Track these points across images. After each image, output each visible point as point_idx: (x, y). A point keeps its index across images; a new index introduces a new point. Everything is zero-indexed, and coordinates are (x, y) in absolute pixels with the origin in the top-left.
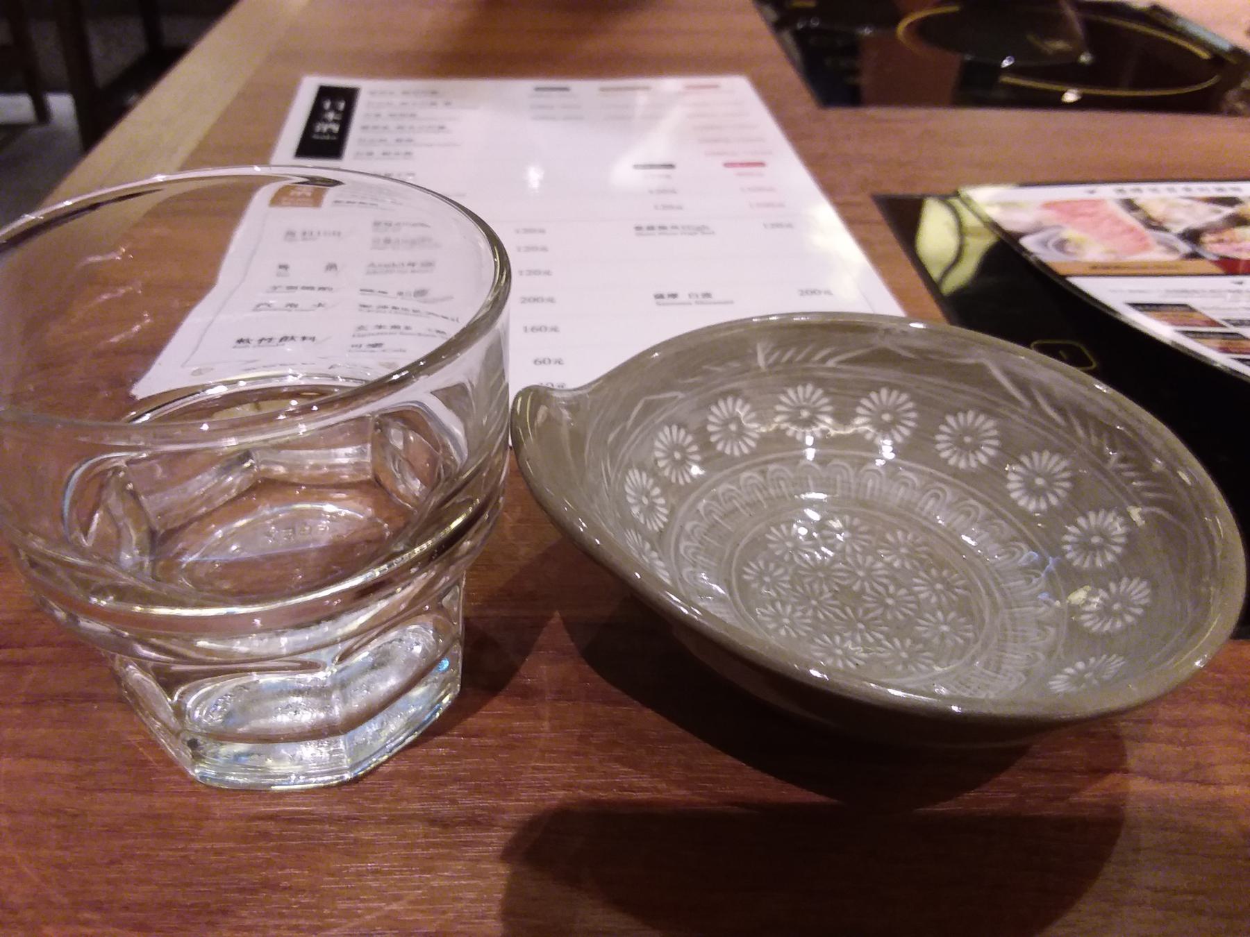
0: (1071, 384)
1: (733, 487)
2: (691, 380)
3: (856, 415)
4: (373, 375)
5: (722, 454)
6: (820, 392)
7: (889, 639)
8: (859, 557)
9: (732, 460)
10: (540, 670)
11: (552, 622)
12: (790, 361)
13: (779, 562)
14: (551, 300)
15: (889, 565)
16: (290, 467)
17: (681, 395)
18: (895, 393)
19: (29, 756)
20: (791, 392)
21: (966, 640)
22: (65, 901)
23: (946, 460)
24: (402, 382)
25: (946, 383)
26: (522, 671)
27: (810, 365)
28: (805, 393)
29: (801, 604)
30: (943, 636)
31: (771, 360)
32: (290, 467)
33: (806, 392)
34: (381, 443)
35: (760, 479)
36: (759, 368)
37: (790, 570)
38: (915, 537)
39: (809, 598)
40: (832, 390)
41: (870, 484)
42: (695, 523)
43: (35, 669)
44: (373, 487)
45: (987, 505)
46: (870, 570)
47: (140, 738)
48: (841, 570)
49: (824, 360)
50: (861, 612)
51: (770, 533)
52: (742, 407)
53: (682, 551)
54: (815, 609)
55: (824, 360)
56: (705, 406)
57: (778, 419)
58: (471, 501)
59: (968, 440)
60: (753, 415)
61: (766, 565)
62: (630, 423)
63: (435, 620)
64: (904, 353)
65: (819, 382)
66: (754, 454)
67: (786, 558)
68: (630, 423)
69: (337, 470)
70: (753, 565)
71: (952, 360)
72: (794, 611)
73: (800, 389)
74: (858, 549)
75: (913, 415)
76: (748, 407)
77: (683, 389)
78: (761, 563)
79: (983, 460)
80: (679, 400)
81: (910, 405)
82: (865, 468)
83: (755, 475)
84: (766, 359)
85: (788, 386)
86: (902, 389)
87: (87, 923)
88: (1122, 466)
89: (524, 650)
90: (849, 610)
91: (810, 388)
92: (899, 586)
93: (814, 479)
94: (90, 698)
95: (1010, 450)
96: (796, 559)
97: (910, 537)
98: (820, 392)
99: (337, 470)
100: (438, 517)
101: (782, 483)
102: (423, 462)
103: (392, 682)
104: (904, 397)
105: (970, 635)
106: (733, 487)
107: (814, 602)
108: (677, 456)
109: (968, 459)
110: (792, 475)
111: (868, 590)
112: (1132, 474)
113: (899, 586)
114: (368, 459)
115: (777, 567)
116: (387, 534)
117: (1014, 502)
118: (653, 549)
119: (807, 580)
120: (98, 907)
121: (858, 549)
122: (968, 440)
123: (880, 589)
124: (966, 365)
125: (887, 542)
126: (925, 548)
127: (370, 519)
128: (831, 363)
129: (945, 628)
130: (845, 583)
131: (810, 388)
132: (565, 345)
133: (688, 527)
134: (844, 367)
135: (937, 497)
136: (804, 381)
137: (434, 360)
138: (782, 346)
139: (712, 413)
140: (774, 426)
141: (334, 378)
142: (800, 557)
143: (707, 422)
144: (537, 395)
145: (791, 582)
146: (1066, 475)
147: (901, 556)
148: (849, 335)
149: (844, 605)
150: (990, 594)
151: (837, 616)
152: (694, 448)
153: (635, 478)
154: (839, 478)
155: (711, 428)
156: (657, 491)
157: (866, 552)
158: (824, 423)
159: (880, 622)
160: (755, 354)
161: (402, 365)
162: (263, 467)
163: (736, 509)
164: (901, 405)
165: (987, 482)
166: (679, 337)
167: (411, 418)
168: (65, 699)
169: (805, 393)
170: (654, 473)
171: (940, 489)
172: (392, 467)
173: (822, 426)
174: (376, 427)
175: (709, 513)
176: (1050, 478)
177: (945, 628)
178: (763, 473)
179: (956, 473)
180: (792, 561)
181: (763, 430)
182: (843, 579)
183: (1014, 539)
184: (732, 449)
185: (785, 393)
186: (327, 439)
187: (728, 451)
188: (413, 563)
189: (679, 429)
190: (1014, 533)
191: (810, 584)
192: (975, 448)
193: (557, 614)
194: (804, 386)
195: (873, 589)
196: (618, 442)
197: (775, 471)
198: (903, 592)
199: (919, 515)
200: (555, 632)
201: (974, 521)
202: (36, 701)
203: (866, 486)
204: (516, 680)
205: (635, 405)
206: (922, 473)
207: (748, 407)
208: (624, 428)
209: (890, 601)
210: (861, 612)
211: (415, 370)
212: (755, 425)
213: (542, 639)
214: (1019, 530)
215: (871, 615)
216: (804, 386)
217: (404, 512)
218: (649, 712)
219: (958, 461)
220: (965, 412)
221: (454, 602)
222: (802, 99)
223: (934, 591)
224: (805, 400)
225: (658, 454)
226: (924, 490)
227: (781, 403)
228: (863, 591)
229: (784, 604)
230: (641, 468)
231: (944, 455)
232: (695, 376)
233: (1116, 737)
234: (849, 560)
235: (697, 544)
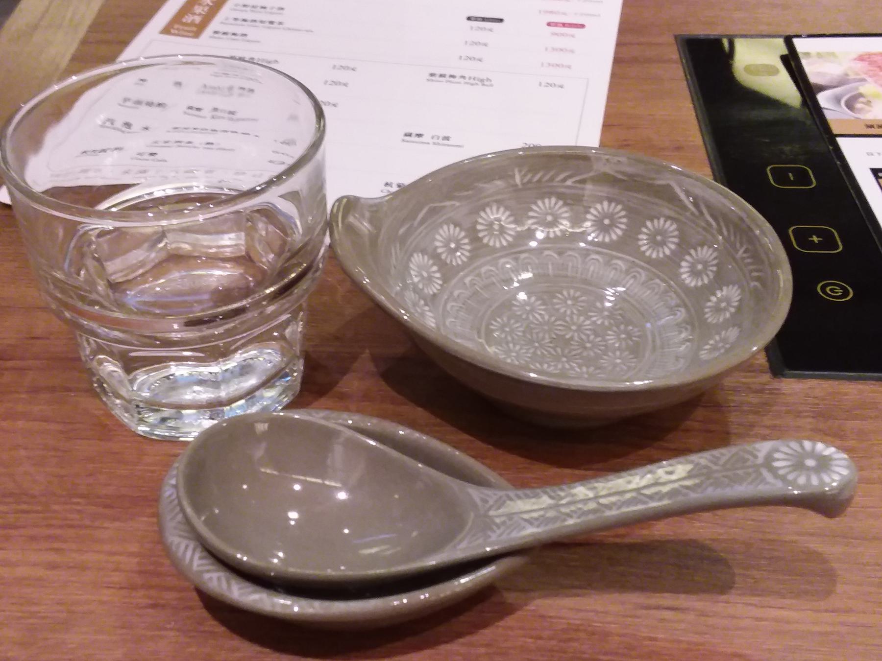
0: (721, 198)
1: (493, 268)
2: (466, 193)
3: (586, 220)
4: (245, 187)
5: (487, 245)
6: (561, 203)
8: (575, 317)
9: (494, 250)
10: (351, 383)
11: (363, 356)
12: (539, 181)
13: (518, 318)
14: (569, 67)
15: (594, 323)
16: (193, 245)
17: (457, 204)
18: (613, 205)
19: (34, 420)
20: (540, 203)
22: (64, 493)
23: (644, 252)
24: (263, 191)
25: (645, 197)
26: (339, 385)
27: (555, 184)
28: (550, 203)
29: (526, 345)
30: (615, 365)
31: (526, 180)
32: (193, 245)
33: (551, 202)
34: (250, 232)
36: (516, 185)
37: (525, 325)
39: (534, 342)
40: (569, 201)
41: (592, 268)
43: (31, 372)
44: (245, 260)
46: (580, 326)
47: (101, 412)
49: (564, 180)
50: (566, 351)
52: (504, 212)
53: (448, 307)
54: (536, 348)
55: (564, 180)
57: (530, 222)
58: (301, 264)
59: (659, 238)
60: (512, 219)
61: (509, 319)
62: (416, 223)
63: (282, 346)
64: (620, 176)
65: (560, 196)
66: (511, 245)
67: (524, 316)
68: (416, 223)
69: (222, 250)
70: (499, 320)
71: (651, 182)
72: (521, 349)
73: (547, 201)
74: (575, 312)
75: (624, 220)
76: (508, 213)
77: (459, 199)
78: (505, 319)
79: (668, 252)
80: (456, 207)
81: (623, 213)
82: (589, 258)
84: (522, 180)
85: (537, 198)
86: (618, 202)
87: (78, 504)
88: (745, 255)
89: (344, 371)
91: (553, 200)
92: (597, 336)
93: (553, 264)
94: (68, 390)
95: (685, 246)
96: (531, 318)
98: (561, 203)
99: (222, 250)
100: (283, 273)
102: (277, 244)
103: (252, 381)
104: (619, 207)
106: (493, 268)
107: (537, 344)
109: (658, 252)
110: (537, 261)
111: (576, 338)
112: (749, 261)
113: (597, 336)
114: (242, 242)
115: (517, 322)
116: (252, 284)
118: (426, 305)
119: (534, 331)
120: (82, 496)
121: (575, 312)
122: (659, 238)
123: (584, 337)
124: (659, 186)
125: (596, 308)
126: (620, 312)
127: (241, 274)
128: (569, 183)
131: (553, 200)
132: (364, 168)
133: (456, 293)
134: (578, 185)
135: (634, 277)
136: (549, 195)
137: (278, 179)
138: (533, 170)
139: (481, 217)
140: (526, 227)
141: (222, 189)
142: (534, 316)
143: (477, 222)
144: (349, 204)
145: (524, 332)
146: (715, 262)
147: (604, 318)
148: (581, 162)
151: (550, 353)
152: (466, 241)
153: (418, 259)
154: (570, 264)
155: (479, 227)
156: (435, 268)
157: (580, 313)
158: (562, 224)
160: (513, 177)
161: (262, 182)
162: (174, 246)
163: (494, 284)
164: (618, 213)
165: (667, 267)
166: (448, 166)
167: (268, 213)
168: (52, 389)
169: (550, 203)
170: (436, 257)
171: (638, 272)
172: (259, 248)
173: (562, 227)
174: (248, 220)
175: (473, 284)
176: (705, 264)
179: (649, 261)
180: (527, 318)
181: (519, 229)
183: (678, 306)
184: (495, 242)
186: (215, 228)
187: (491, 244)
188: (264, 299)
189: (455, 227)
190: (678, 301)
192: (663, 243)
193: (367, 351)
194: (550, 198)
196: (408, 233)
197: (525, 258)
198: (599, 339)
200: (365, 362)
201: (656, 294)
202: (35, 390)
203: (588, 270)
204: (336, 389)
205: (421, 210)
206: (628, 261)
207: (508, 213)
208: (413, 224)
209: (588, 345)
210: (566, 351)
211: (270, 183)
212: (513, 226)
213: (356, 365)
214: (683, 301)
215: (574, 353)
216: (550, 198)
217: (263, 272)
218: (420, 409)
219: (652, 253)
220: (659, 219)
221: (295, 331)
224: (550, 208)
225: (438, 244)
226: (627, 272)
228: (572, 338)
229: (514, 345)
230: (424, 252)
231: (643, 248)
232: (467, 191)
233: (728, 433)
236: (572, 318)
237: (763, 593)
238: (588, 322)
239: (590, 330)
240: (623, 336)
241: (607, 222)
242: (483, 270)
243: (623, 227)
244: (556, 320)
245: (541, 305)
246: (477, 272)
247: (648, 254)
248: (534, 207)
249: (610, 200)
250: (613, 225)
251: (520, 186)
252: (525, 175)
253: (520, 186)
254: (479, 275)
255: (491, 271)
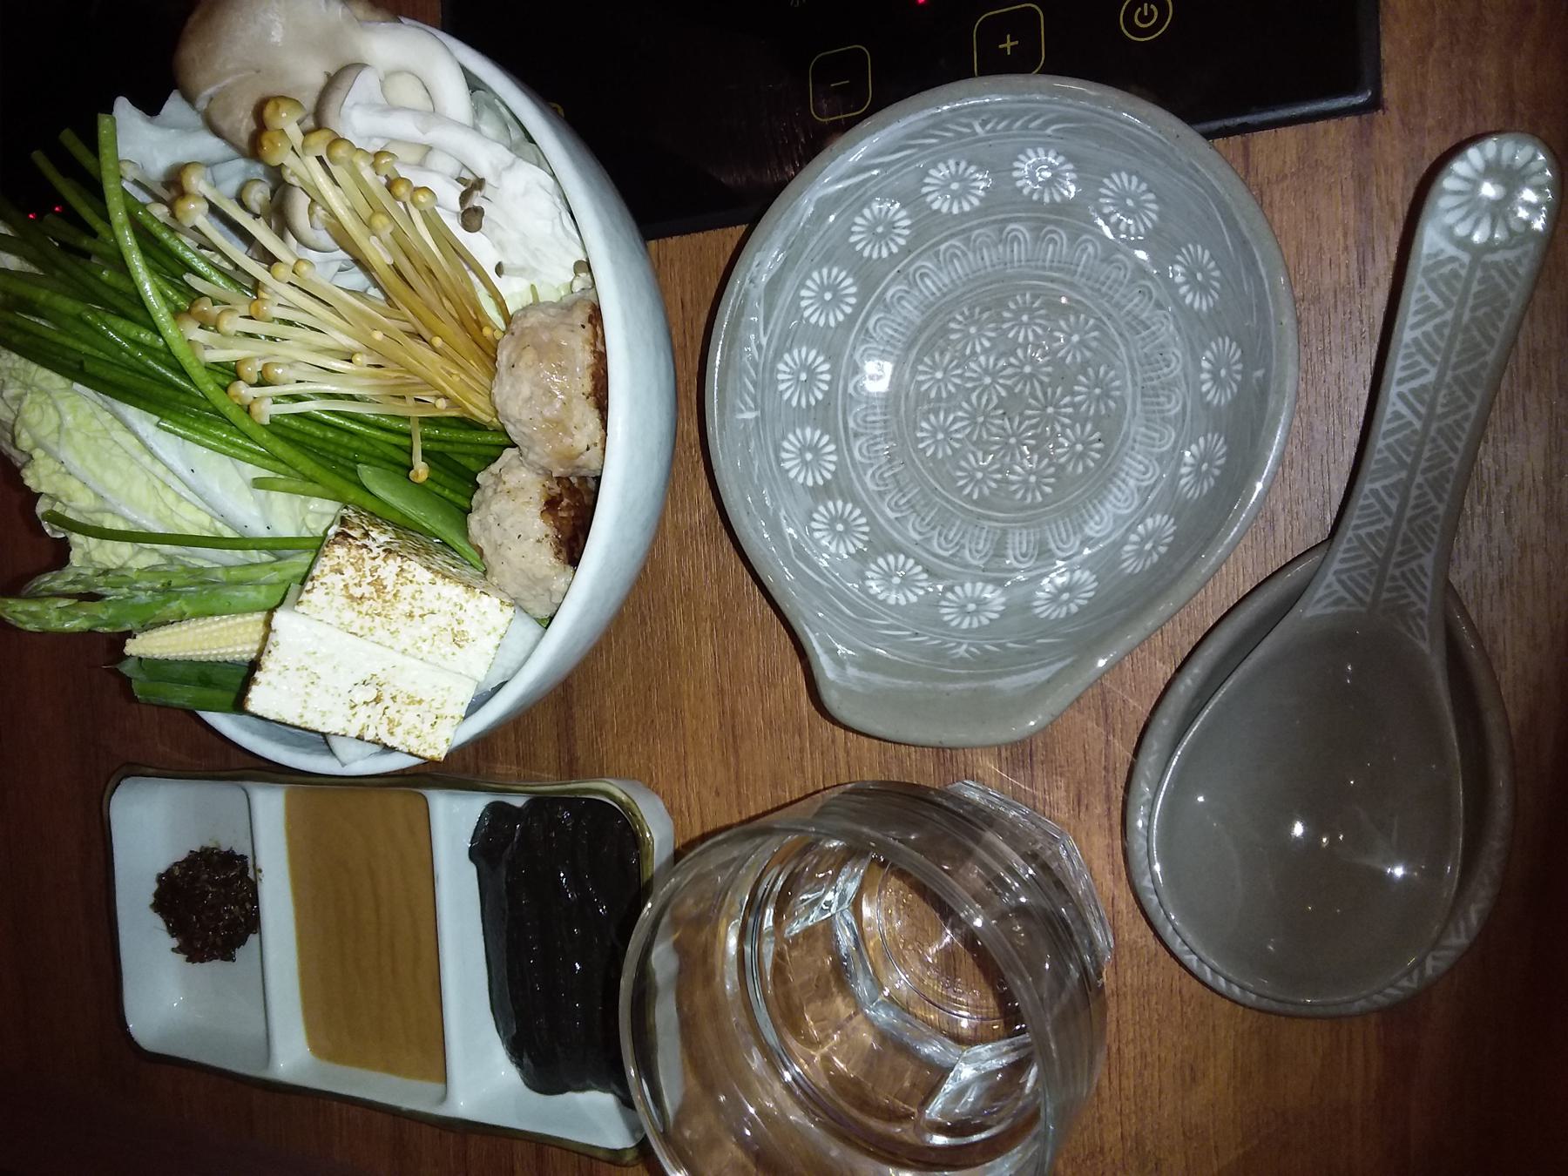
1: (870, 472)
7: (1074, 394)
12: (755, 384)
21: (1095, 328)
30: (1083, 343)
35: (863, 439)
38: (962, 314)
42: (910, 527)
45: (952, 236)
48: (979, 398)
51: (924, 450)
56: (790, 483)
59: (880, 230)
66: (835, 439)
74: (959, 371)
83: (858, 443)
84: (750, 409)
86: (808, 276)
90: (1029, 412)
96: (959, 436)
97: (959, 318)
101: (870, 419)
105: (1092, 322)
108: (840, 527)
117: (963, 214)
121: (959, 371)
122: (880, 230)
123: (1009, 371)
126: (977, 310)
129: (1075, 338)
130: (995, 400)
131: (781, 367)
134: (771, 327)
147: (980, 335)
149: (1021, 414)
150: (1053, 280)
159: (1049, 391)
160: (745, 421)
175: (896, 507)
177: (1075, 338)
178: (856, 435)
182: (988, 401)
183: (1001, 231)
185: (782, 393)
187: (832, 467)
191: (990, 434)
195: (1009, 377)
199: (939, 299)
222: (149, 121)
223: (1027, 325)
227: (790, 399)
234: (969, 385)
235: (936, 533)
236: (971, 379)
237: (1536, 284)
238: (982, 359)
239: (997, 360)
240: (1025, 318)
241: (828, 296)
242: (871, 486)
243: (843, 274)
244: (969, 401)
245: (937, 416)
246: (876, 497)
247: (895, 250)
248: (786, 396)
249: (802, 285)
250: (834, 288)
251: (758, 413)
252: (745, 404)
253: (758, 413)
254: (881, 494)
255: (873, 475)
